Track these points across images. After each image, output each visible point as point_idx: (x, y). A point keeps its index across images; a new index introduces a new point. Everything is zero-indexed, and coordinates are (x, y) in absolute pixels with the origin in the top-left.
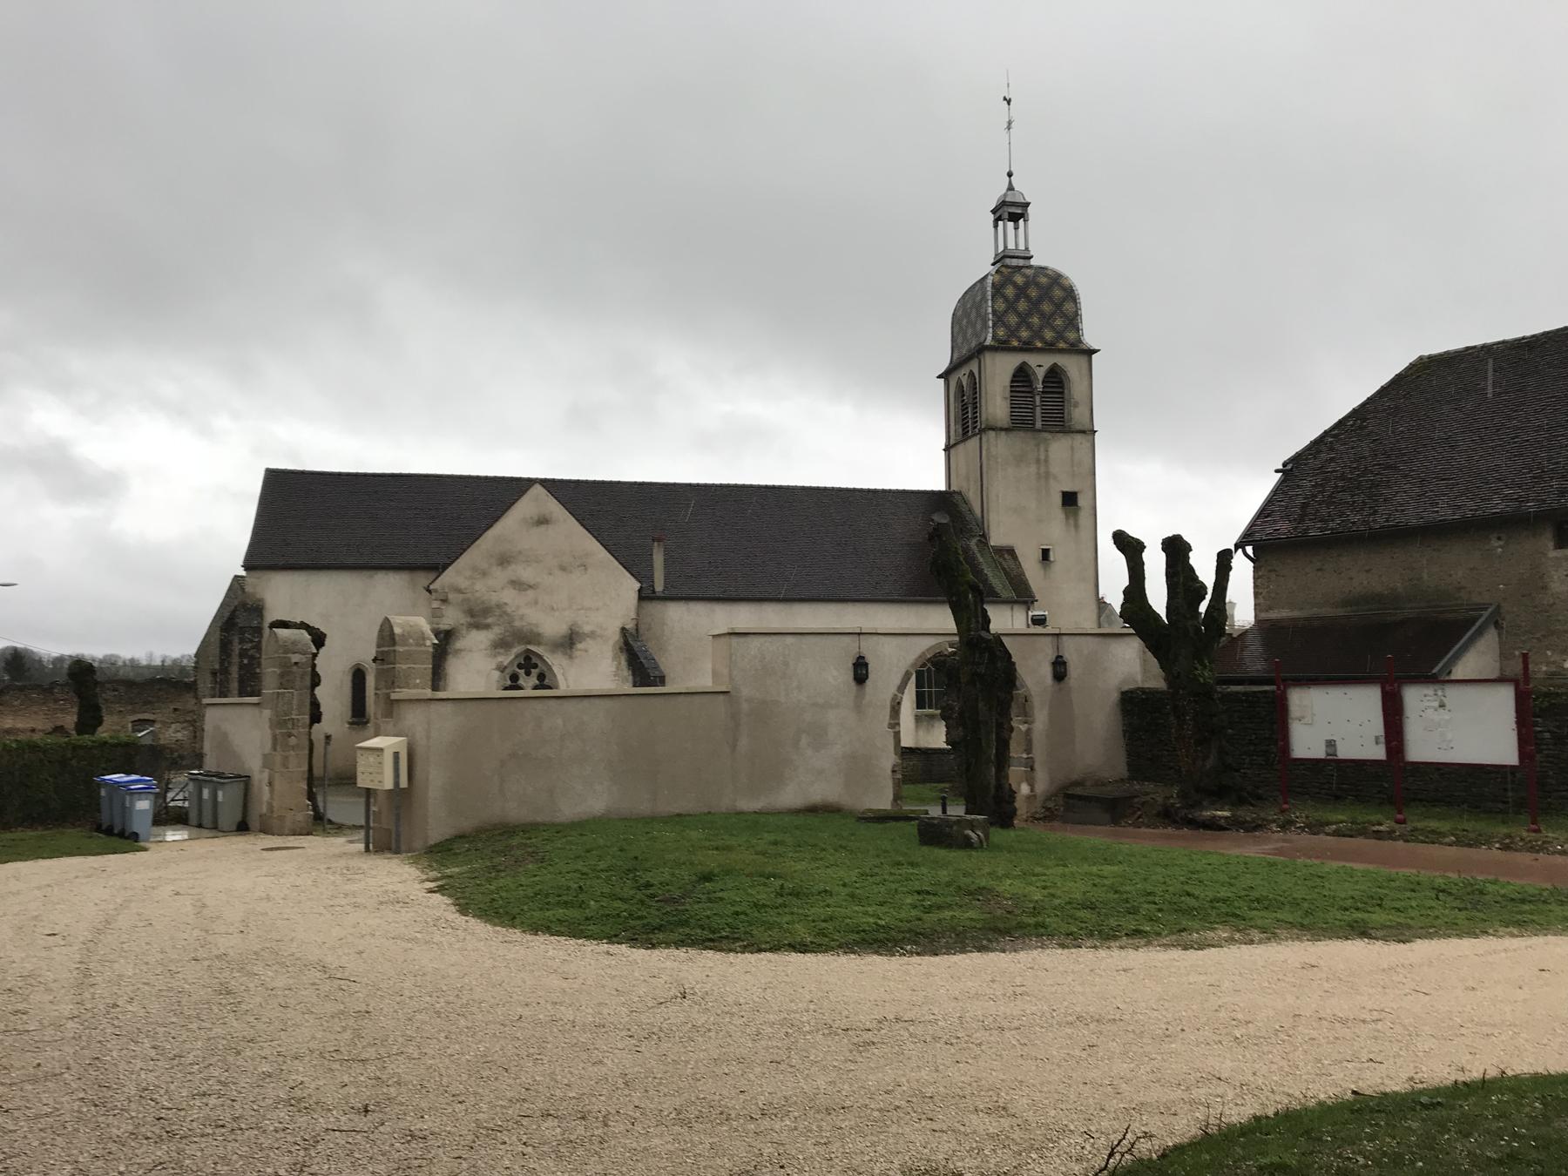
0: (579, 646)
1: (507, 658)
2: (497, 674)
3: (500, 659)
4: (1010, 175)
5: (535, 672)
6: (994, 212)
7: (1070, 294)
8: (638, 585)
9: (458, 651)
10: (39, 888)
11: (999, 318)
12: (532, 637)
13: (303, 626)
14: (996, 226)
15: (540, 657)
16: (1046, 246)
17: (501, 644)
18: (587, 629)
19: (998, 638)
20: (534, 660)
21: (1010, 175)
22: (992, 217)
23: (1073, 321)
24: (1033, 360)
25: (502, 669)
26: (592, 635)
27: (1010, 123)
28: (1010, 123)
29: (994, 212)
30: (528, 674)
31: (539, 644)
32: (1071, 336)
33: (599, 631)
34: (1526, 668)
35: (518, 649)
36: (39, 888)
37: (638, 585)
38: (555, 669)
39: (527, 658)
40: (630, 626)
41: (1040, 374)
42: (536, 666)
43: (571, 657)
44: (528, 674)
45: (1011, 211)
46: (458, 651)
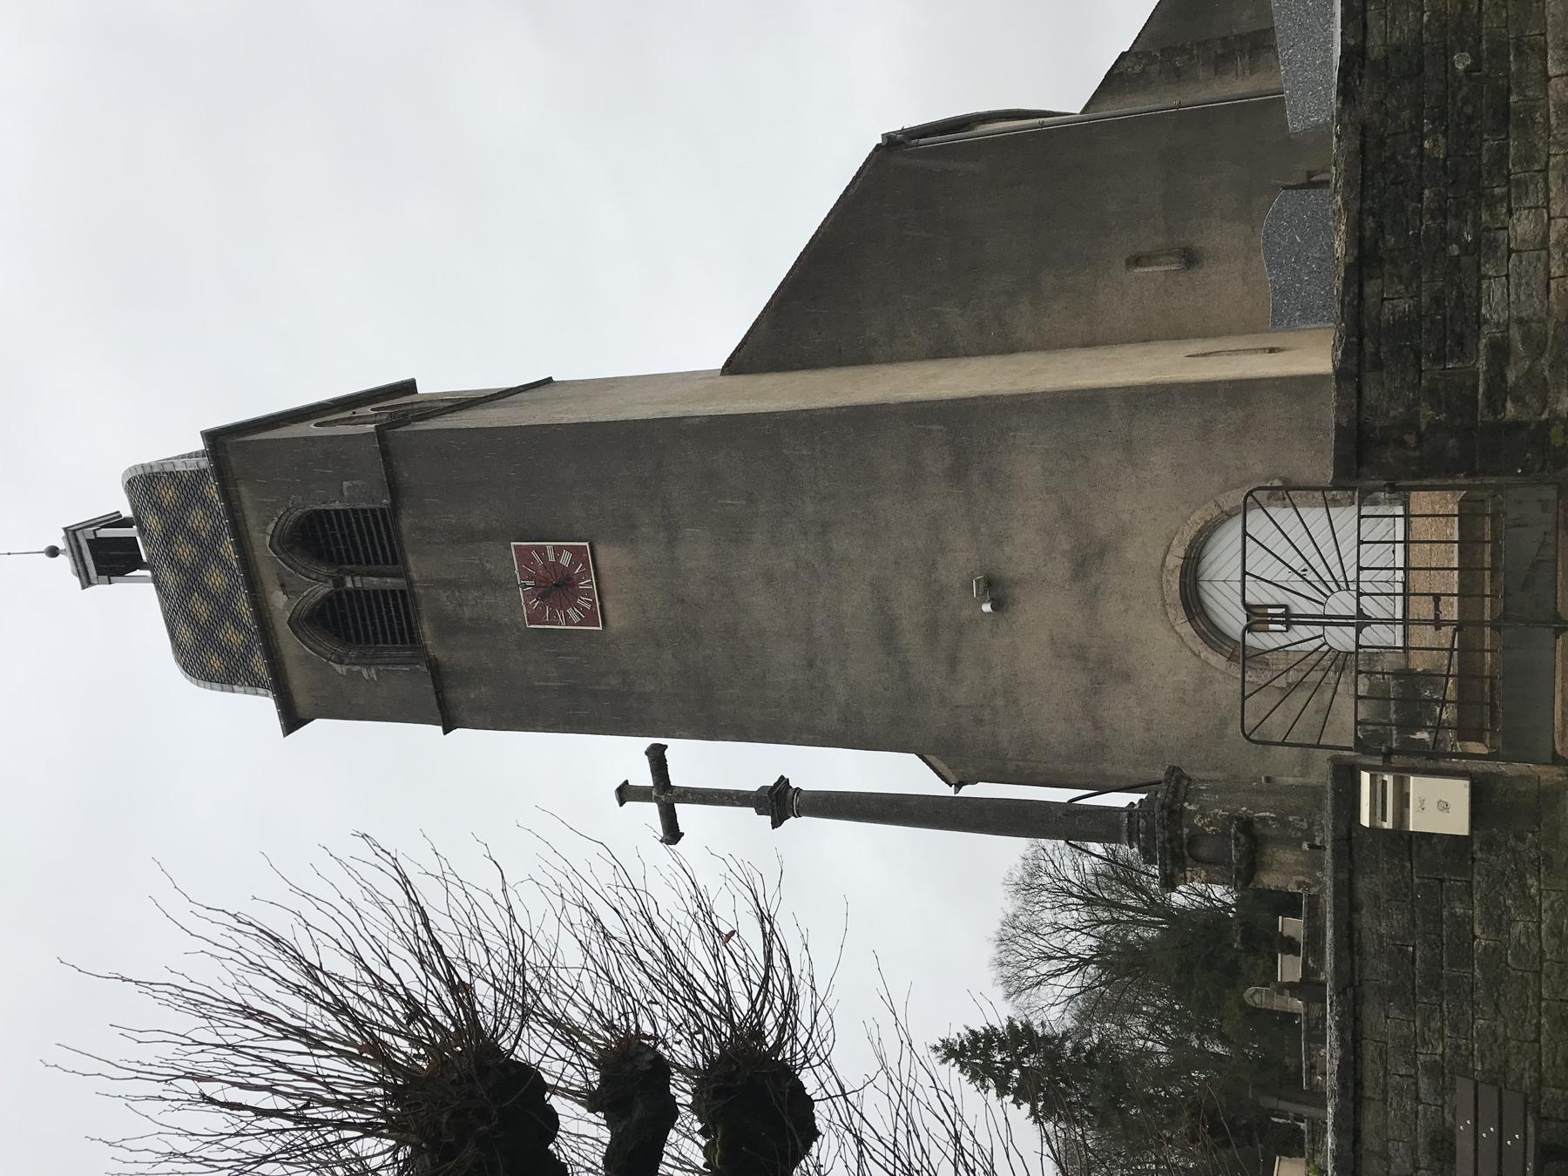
24: (279, 600)
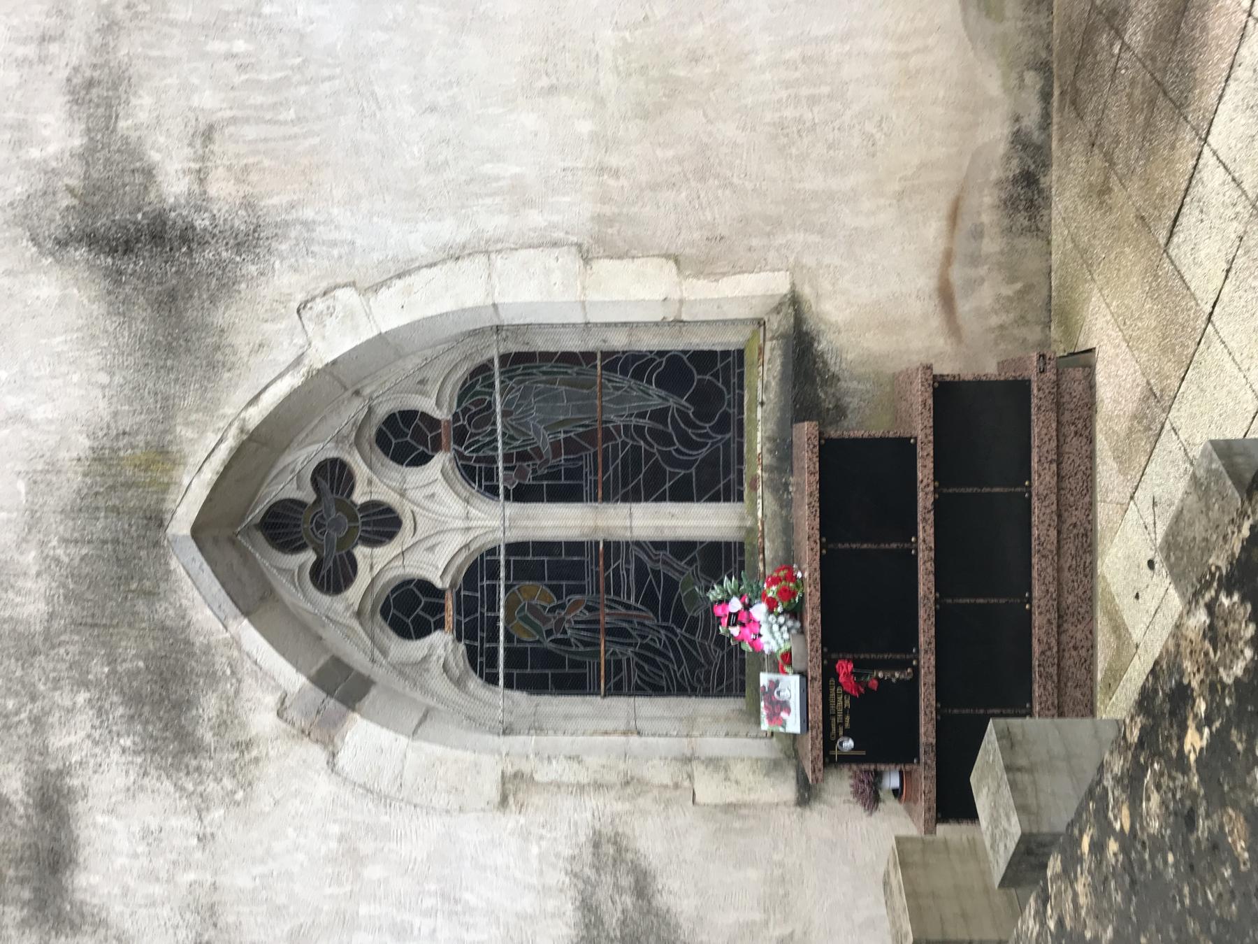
0: (173, 185)
1: (262, 673)
2: (363, 735)
3: (261, 719)
5: (374, 482)
10: (357, 84)
12: (118, 497)
13: (461, 549)
15: (257, 449)
17: (167, 706)
18: (57, 136)
20: (290, 481)
25: (343, 686)
26: (98, 95)
30: (383, 523)
31: (163, 456)
33: (72, 54)
35: (196, 597)
36: (357, 84)
38: (333, 342)
39: (282, 526)
42: (333, 476)
43: (249, 240)
44: (383, 523)
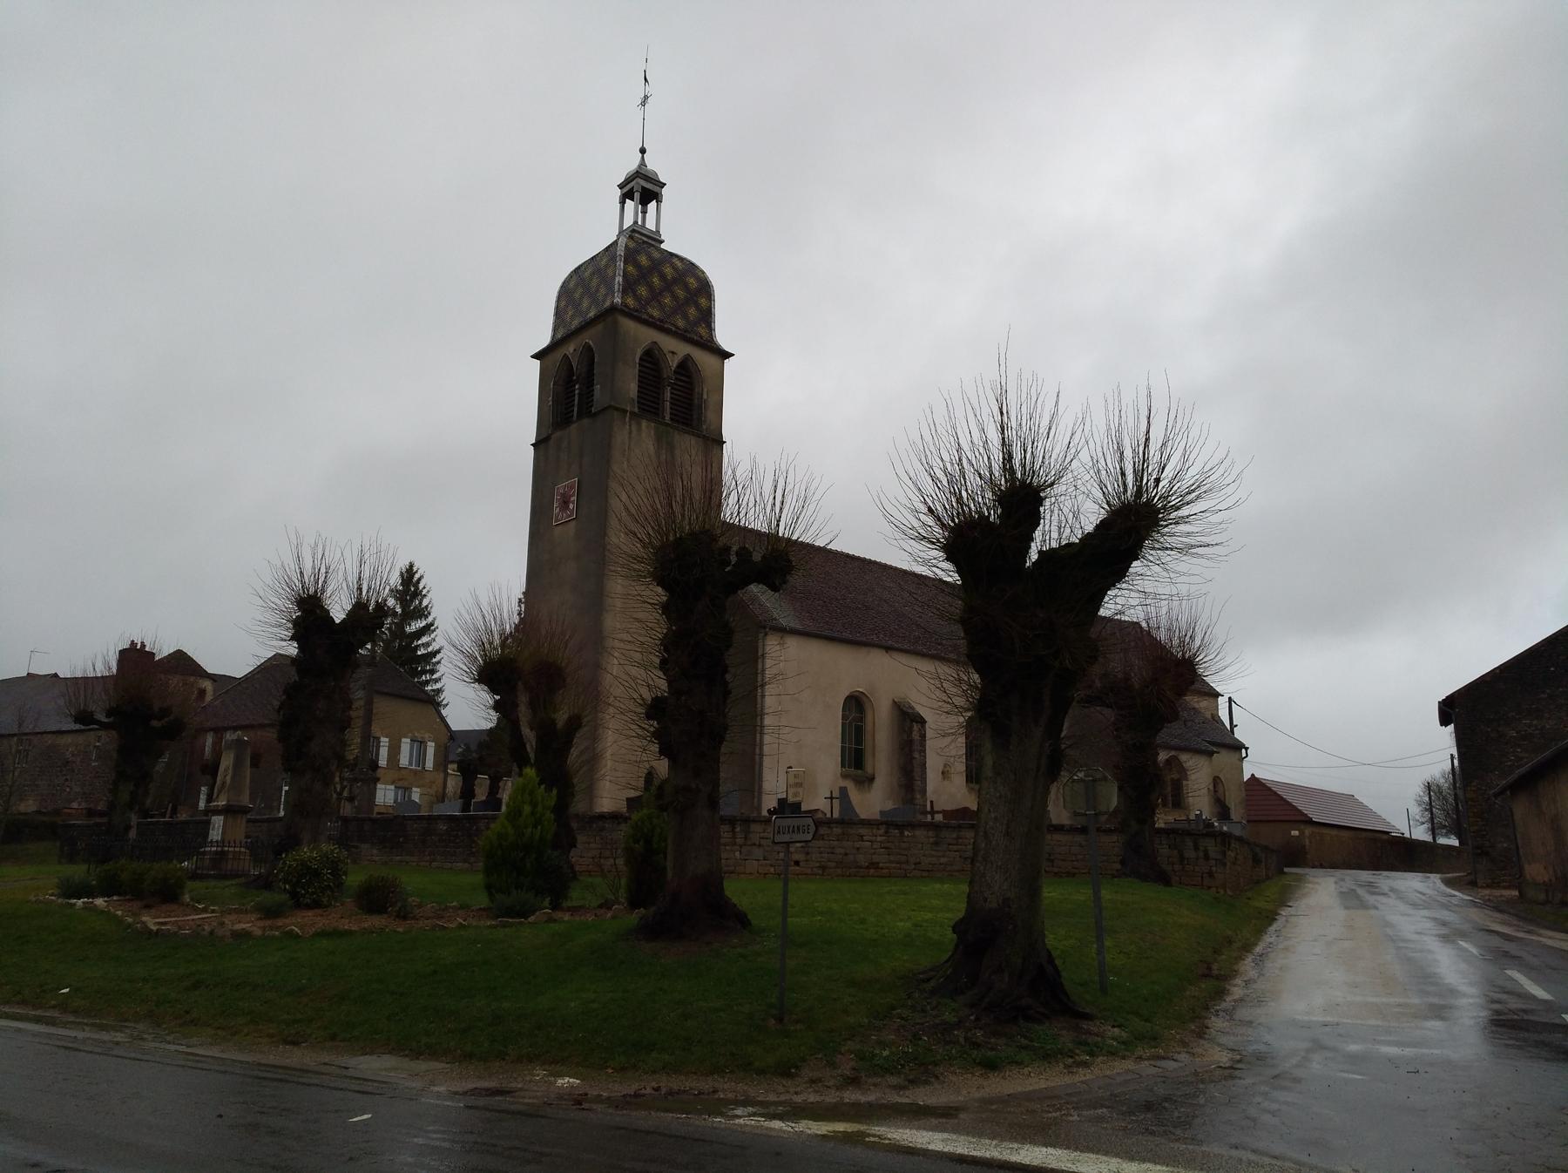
4: (643, 151)
6: (621, 186)
7: (704, 289)
8: (1251, 768)
9: (1182, 643)
11: (629, 287)
14: (623, 203)
16: (681, 231)
19: (661, 583)
21: (643, 151)
22: (618, 192)
23: (707, 316)
24: (668, 343)
27: (643, 103)
28: (643, 103)
29: (621, 186)
32: (702, 331)
34: (785, 899)
37: (1251, 768)
40: (804, 808)
41: (674, 363)
45: (642, 188)
46: (1182, 643)
